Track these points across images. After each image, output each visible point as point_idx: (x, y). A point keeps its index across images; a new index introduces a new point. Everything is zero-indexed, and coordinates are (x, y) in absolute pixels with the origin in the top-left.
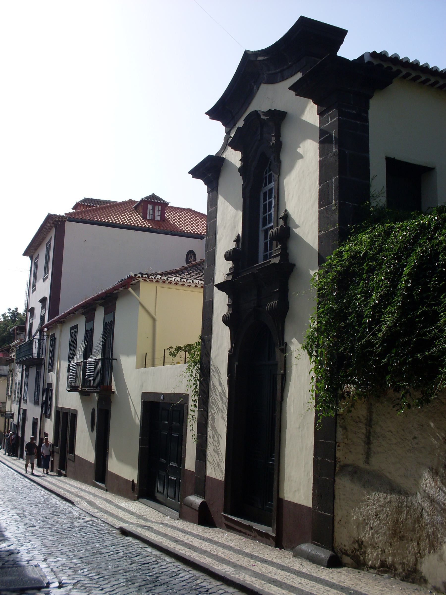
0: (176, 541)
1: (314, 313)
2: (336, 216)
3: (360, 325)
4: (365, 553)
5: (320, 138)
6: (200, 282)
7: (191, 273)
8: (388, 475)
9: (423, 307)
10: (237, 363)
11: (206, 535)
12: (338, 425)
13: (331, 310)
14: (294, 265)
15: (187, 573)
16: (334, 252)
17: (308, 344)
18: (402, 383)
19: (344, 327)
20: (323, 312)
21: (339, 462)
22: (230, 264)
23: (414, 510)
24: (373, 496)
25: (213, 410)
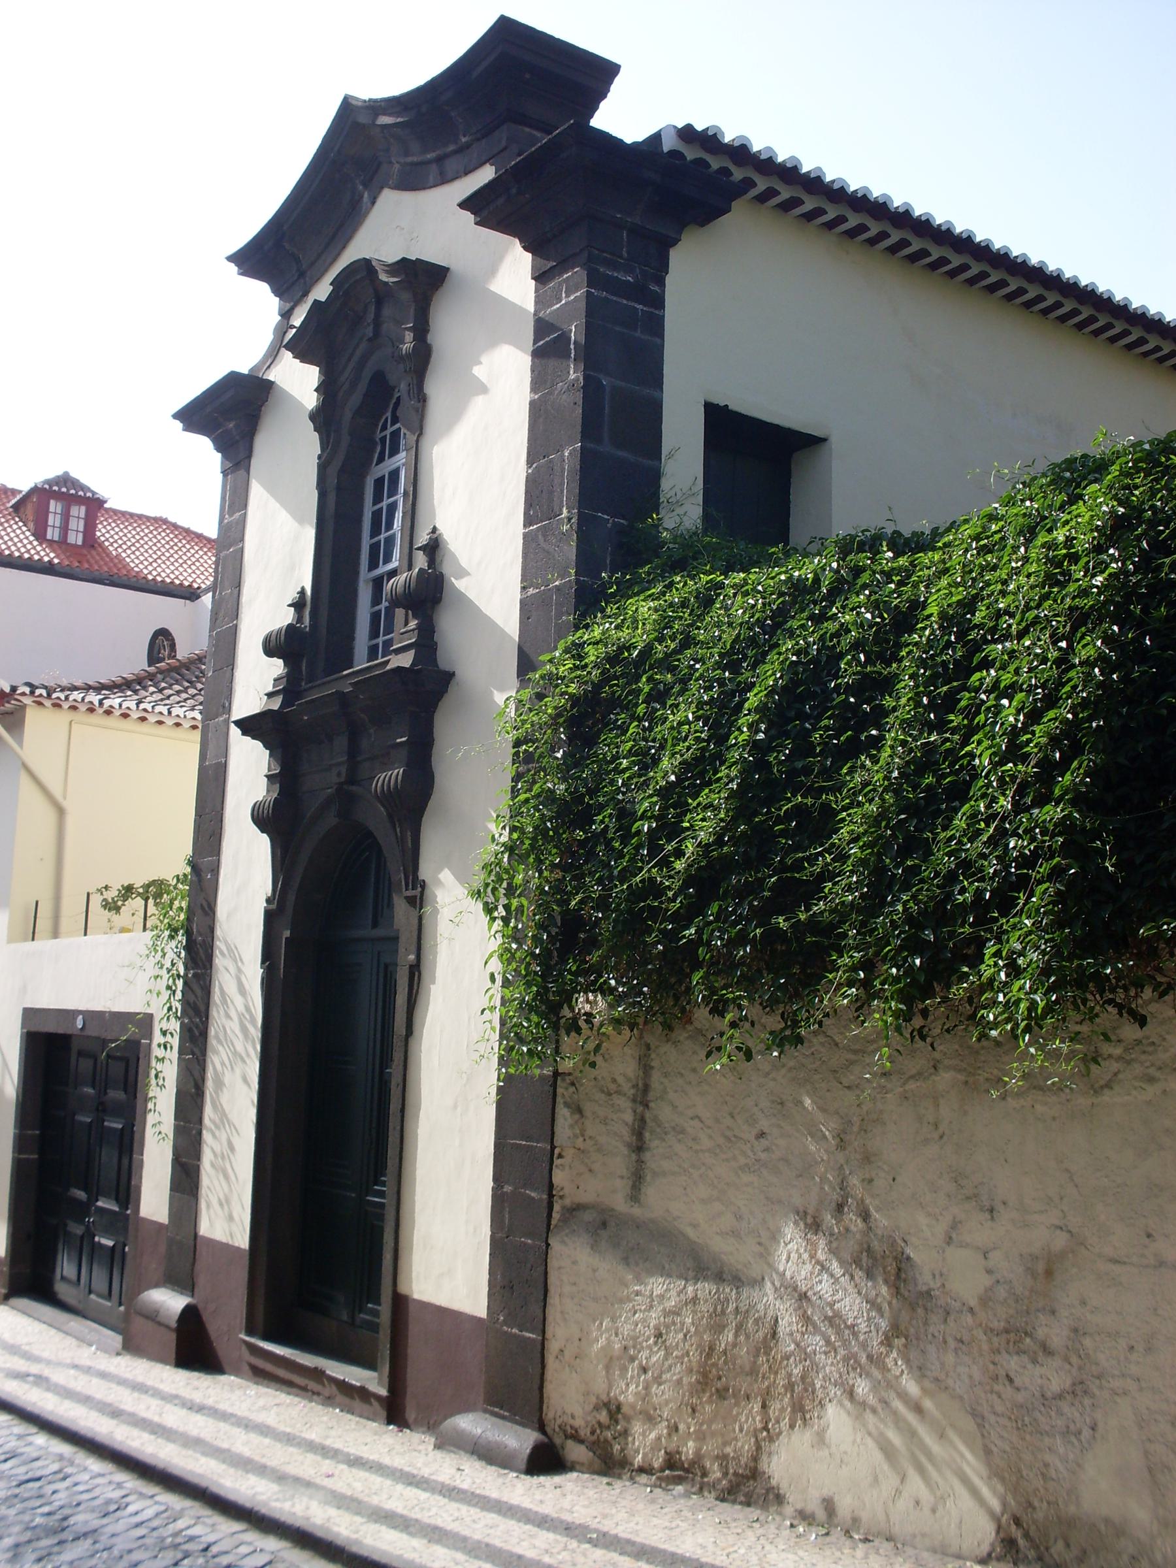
0: (116, 1413)
1: (505, 802)
2: (570, 551)
3: (625, 840)
4: (625, 1433)
5: (535, 342)
6: (190, 714)
7: (164, 688)
8: (690, 1232)
9: (794, 795)
10: (287, 933)
11: (197, 1397)
12: (559, 1099)
13: (549, 797)
14: (449, 676)
15: (149, 1502)
16: (561, 645)
17: (487, 885)
18: (732, 992)
19: (582, 844)
20: (527, 801)
21: (561, 1197)
22: (277, 667)
23: (756, 1321)
24: (649, 1288)
25: (218, 1059)
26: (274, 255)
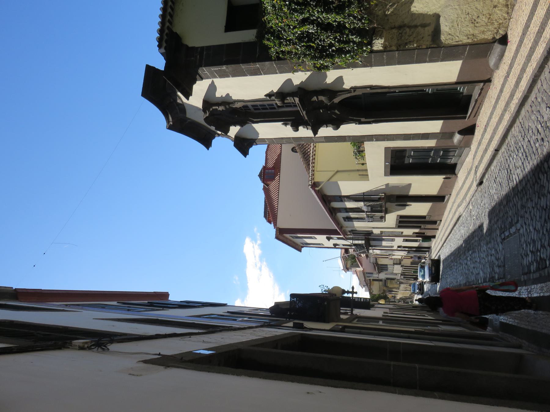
0: (486, 150)
22: (301, 128)
26: (206, 140)
